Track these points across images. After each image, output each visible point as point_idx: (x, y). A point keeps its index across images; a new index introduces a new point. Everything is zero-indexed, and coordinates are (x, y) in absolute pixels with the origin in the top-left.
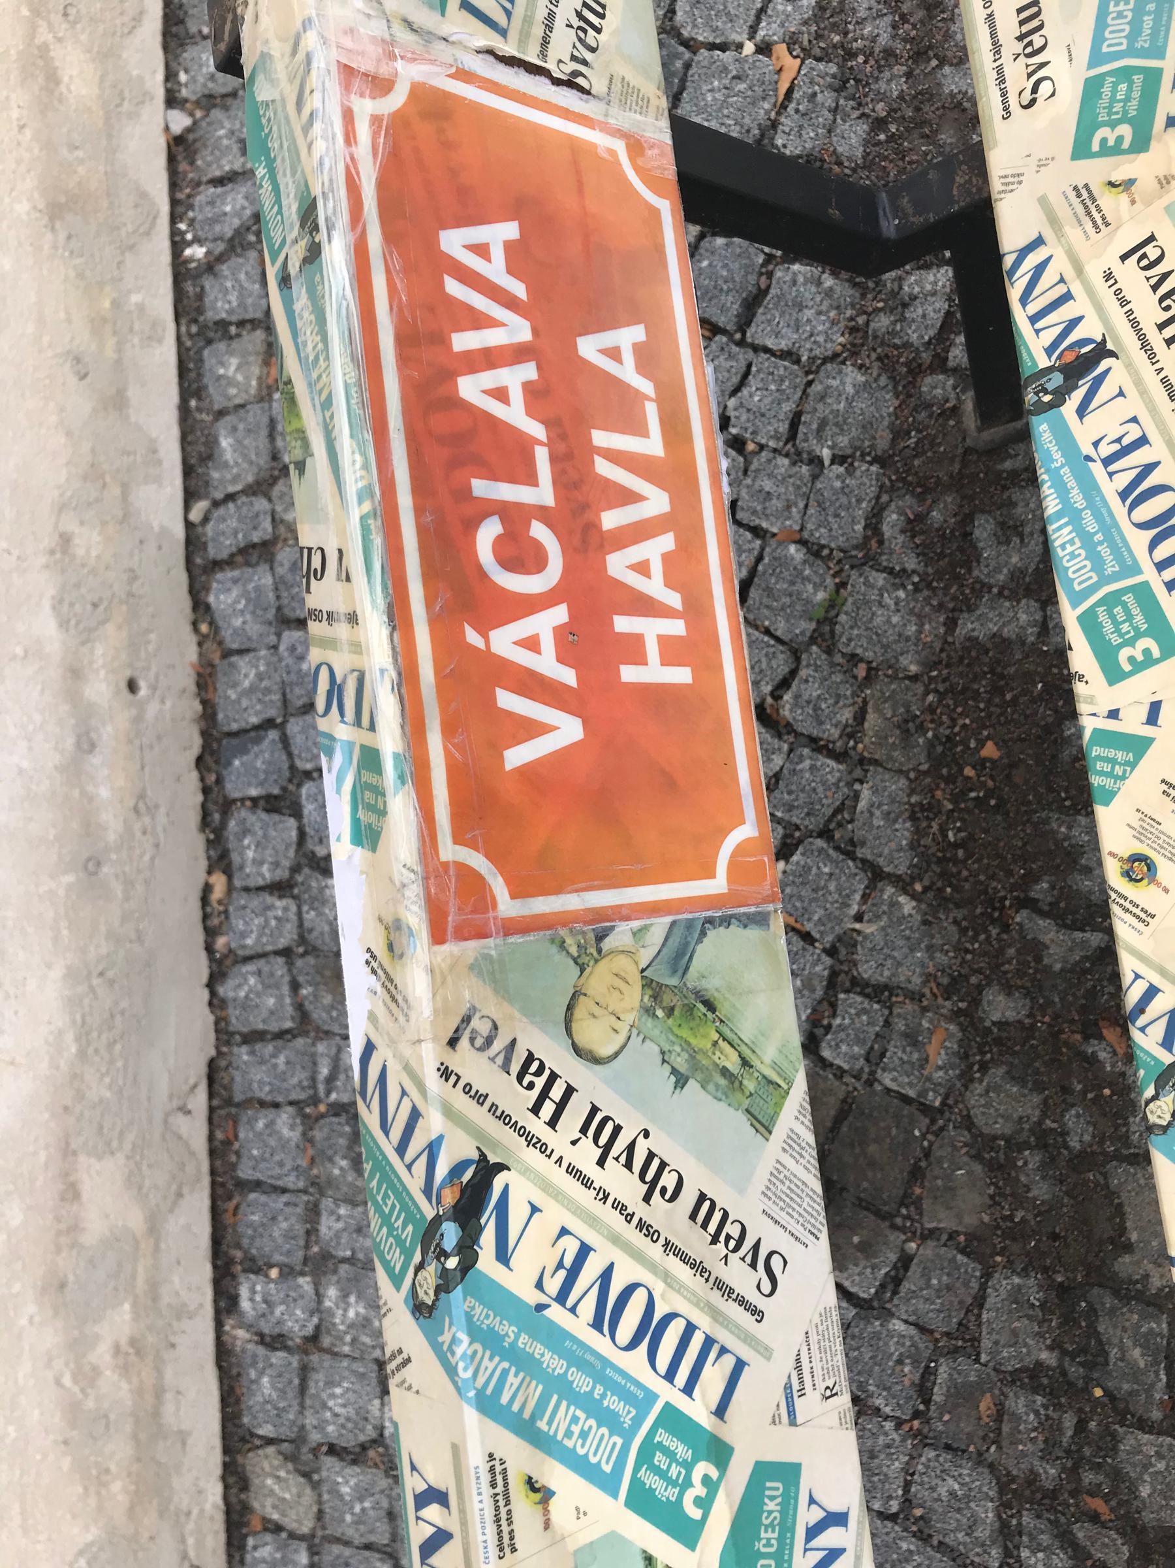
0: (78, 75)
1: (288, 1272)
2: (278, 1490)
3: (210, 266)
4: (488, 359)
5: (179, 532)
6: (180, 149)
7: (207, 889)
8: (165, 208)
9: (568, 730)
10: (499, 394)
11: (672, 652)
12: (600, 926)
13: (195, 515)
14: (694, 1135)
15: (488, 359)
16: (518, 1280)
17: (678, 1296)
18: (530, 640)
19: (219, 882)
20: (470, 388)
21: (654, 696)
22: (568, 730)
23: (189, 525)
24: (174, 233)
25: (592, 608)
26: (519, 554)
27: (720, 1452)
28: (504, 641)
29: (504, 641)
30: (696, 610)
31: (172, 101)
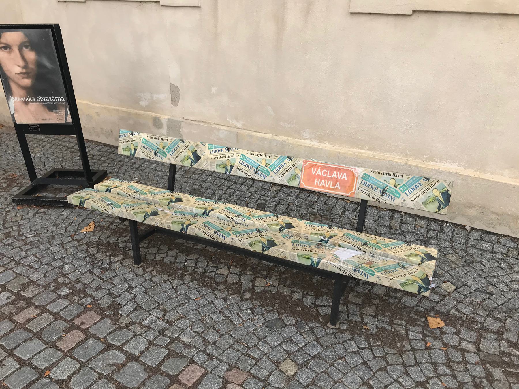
0: (472, 212)
1: (298, 195)
2: (275, 188)
3: (441, 226)
4: (337, 175)
5: (400, 210)
6: (463, 227)
7: (348, 200)
8: (453, 222)
9: (313, 173)
10: (335, 175)
11: (317, 183)
12: (301, 172)
13: (402, 213)
14: (288, 175)
15: (337, 175)
16: (286, 161)
17: (281, 171)
18: (319, 172)
19: (349, 202)
20: (335, 172)
21: (314, 181)
22: (313, 173)
23: (401, 212)
24: (450, 223)
25: (320, 178)
26: (325, 173)
27: (272, 171)
28: (319, 170)
29: (319, 170)
30: (318, 187)
31: (472, 228)
